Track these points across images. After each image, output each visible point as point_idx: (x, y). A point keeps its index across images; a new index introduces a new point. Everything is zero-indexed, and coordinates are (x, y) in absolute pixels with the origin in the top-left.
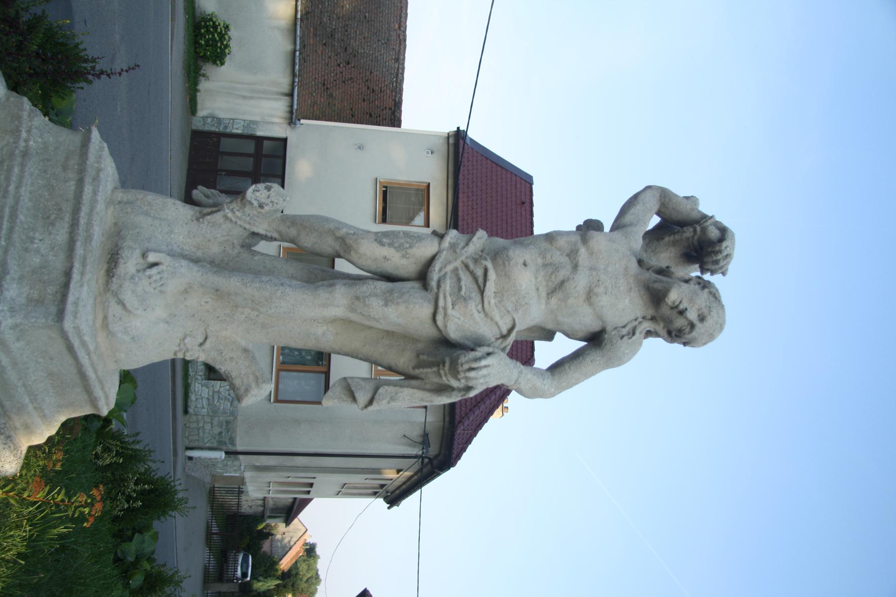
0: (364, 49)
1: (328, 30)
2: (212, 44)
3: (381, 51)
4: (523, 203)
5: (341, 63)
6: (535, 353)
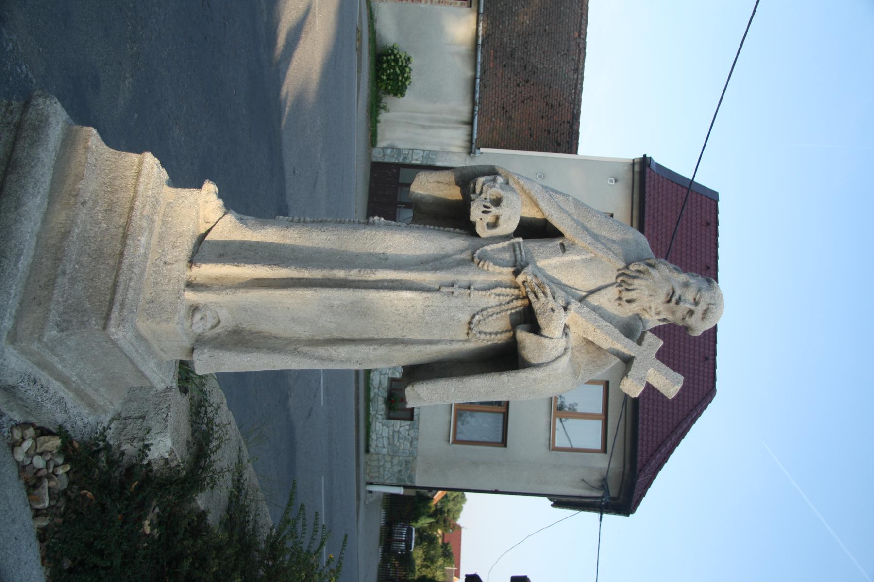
0: (543, 64)
1: (508, 50)
2: (394, 78)
3: (560, 64)
4: (708, 224)
5: (520, 82)
6: (717, 383)
